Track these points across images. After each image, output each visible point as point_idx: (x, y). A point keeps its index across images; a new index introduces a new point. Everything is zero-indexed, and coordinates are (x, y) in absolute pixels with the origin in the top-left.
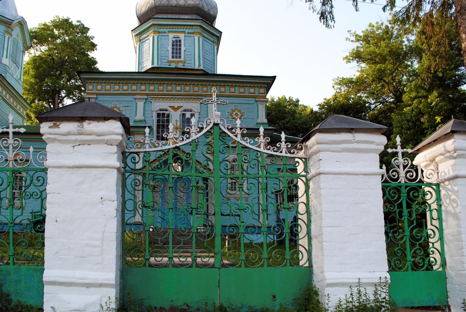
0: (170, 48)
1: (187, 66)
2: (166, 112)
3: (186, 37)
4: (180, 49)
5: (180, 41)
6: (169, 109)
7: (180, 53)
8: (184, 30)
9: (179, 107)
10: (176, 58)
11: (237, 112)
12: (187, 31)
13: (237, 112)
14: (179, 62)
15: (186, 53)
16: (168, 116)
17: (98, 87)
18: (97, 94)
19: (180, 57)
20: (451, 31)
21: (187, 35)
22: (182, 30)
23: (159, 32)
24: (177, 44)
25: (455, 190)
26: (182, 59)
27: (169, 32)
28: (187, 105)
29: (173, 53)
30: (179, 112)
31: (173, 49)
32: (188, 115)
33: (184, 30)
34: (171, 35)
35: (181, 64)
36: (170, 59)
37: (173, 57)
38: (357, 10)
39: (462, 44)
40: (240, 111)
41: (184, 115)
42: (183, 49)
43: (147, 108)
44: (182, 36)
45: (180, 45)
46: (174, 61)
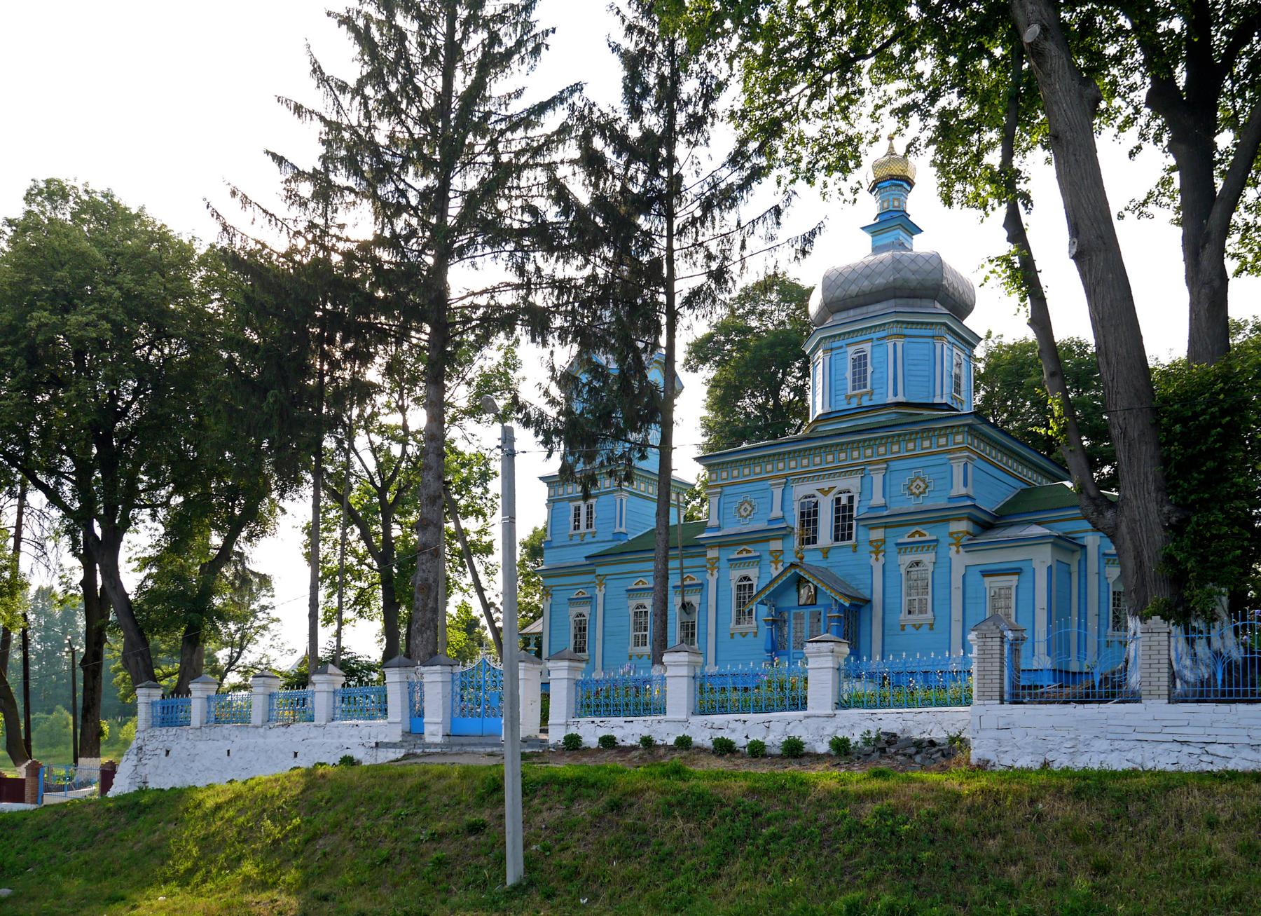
0: (849, 375)
3: (875, 349)
5: (865, 356)
9: (831, 489)
11: (918, 482)
12: (875, 336)
13: (918, 482)
14: (862, 395)
15: (875, 376)
18: (722, 486)
19: (865, 386)
20: (1049, 75)
21: (876, 343)
22: (864, 337)
23: (905, 336)
24: (860, 363)
26: (869, 388)
27: (848, 345)
28: (841, 483)
29: (854, 381)
30: (831, 497)
31: (854, 374)
34: (851, 350)
36: (850, 392)
37: (854, 389)
38: (268, 152)
39: (677, 209)
41: (838, 500)
42: (870, 369)
43: (786, 497)
44: (867, 347)
45: (865, 365)
46: (855, 396)
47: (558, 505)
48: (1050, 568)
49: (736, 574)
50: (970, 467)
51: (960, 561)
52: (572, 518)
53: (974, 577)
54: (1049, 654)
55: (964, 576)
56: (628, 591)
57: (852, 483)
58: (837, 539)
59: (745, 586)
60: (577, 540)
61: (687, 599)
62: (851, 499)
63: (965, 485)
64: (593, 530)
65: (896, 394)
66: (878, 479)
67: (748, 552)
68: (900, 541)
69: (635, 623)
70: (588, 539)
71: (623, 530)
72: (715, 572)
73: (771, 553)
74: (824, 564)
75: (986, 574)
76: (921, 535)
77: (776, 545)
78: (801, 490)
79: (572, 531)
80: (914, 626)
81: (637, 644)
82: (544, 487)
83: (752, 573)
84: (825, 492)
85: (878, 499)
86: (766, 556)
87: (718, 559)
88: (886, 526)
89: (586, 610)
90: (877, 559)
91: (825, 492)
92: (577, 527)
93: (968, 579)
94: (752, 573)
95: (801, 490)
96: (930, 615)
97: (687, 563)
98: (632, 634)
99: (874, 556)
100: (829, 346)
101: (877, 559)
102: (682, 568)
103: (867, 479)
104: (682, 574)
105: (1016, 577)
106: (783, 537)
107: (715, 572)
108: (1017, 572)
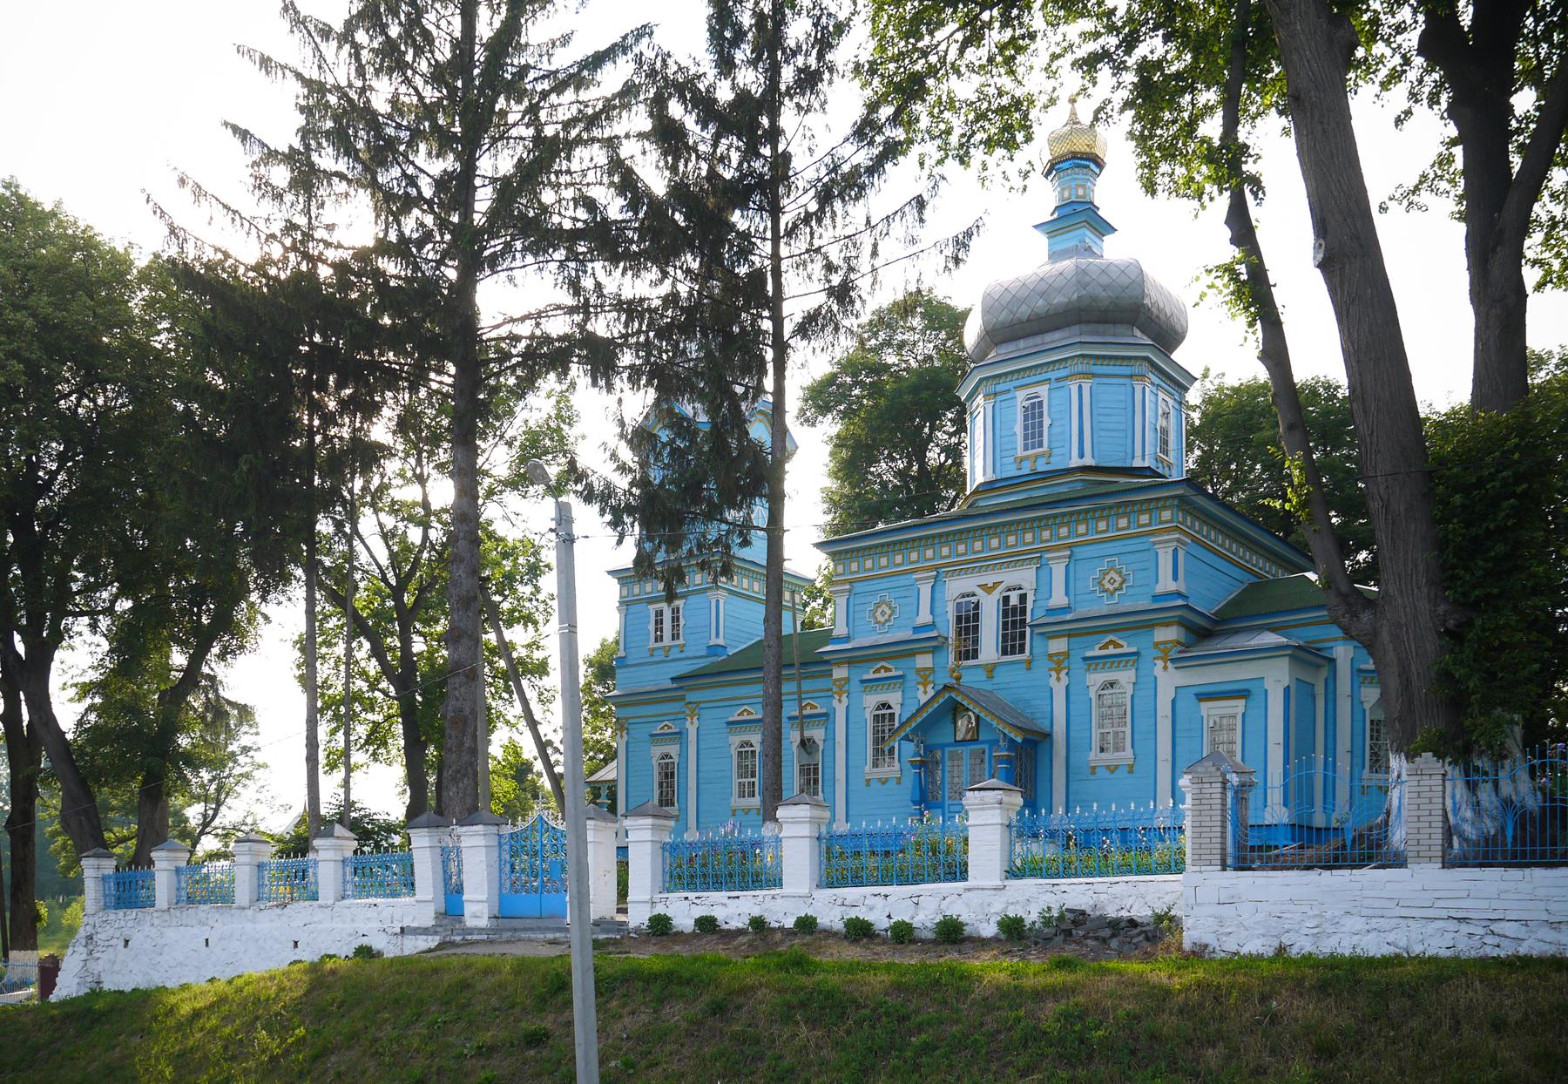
0: (1019, 429)
1: (1057, 463)
2: (974, 599)
3: (1054, 394)
4: (1041, 424)
6: (979, 591)
7: (1041, 435)
8: (1048, 375)
9: (996, 584)
10: (1013, 653)
11: (1113, 574)
12: (1054, 375)
13: (1113, 574)
14: (1037, 457)
16: (977, 606)
17: (757, 613)
18: (851, 582)
19: (1041, 445)
21: (1055, 385)
24: (1033, 412)
25: (315, 837)
26: (1045, 448)
28: (1010, 577)
29: (1026, 438)
30: (997, 595)
31: (1026, 428)
32: (1014, 600)
33: (1048, 375)
34: (1021, 395)
35: (1044, 460)
36: (1020, 453)
37: (1026, 449)
40: (1120, 573)
41: (1006, 600)
42: (1046, 422)
44: (1043, 391)
46: (1027, 457)
47: (633, 608)
48: (1287, 690)
49: (871, 700)
50: (1181, 553)
51: (1168, 680)
52: (652, 627)
53: (1187, 702)
54: (1285, 805)
55: (1174, 701)
56: (729, 723)
57: (1024, 577)
58: (1004, 653)
59: (883, 716)
60: (659, 656)
61: (807, 734)
62: (1023, 598)
63: (1175, 578)
64: (681, 641)
65: (1081, 456)
66: (1059, 571)
67: (750, 713)
68: (1089, 654)
69: (740, 766)
70: (674, 654)
71: (721, 641)
72: (844, 697)
73: (918, 671)
74: (988, 686)
75: (1203, 697)
76: (1117, 646)
77: (924, 661)
78: (957, 586)
79: (652, 644)
80: (1108, 767)
81: (742, 795)
82: (614, 584)
83: (894, 698)
84: (988, 589)
85: (1059, 598)
86: (911, 676)
87: (848, 680)
88: (1070, 634)
89: (673, 750)
90: (1058, 679)
91: (988, 589)
92: (659, 639)
93: (1178, 704)
94: (894, 698)
95: (957, 586)
96: (1129, 753)
97: (807, 685)
98: (735, 781)
99: (1054, 674)
100: (991, 389)
101: (1058, 679)
102: (800, 693)
103: (1044, 572)
104: (800, 700)
105: (1241, 702)
106: (934, 650)
107: (844, 697)
108: (1243, 694)
